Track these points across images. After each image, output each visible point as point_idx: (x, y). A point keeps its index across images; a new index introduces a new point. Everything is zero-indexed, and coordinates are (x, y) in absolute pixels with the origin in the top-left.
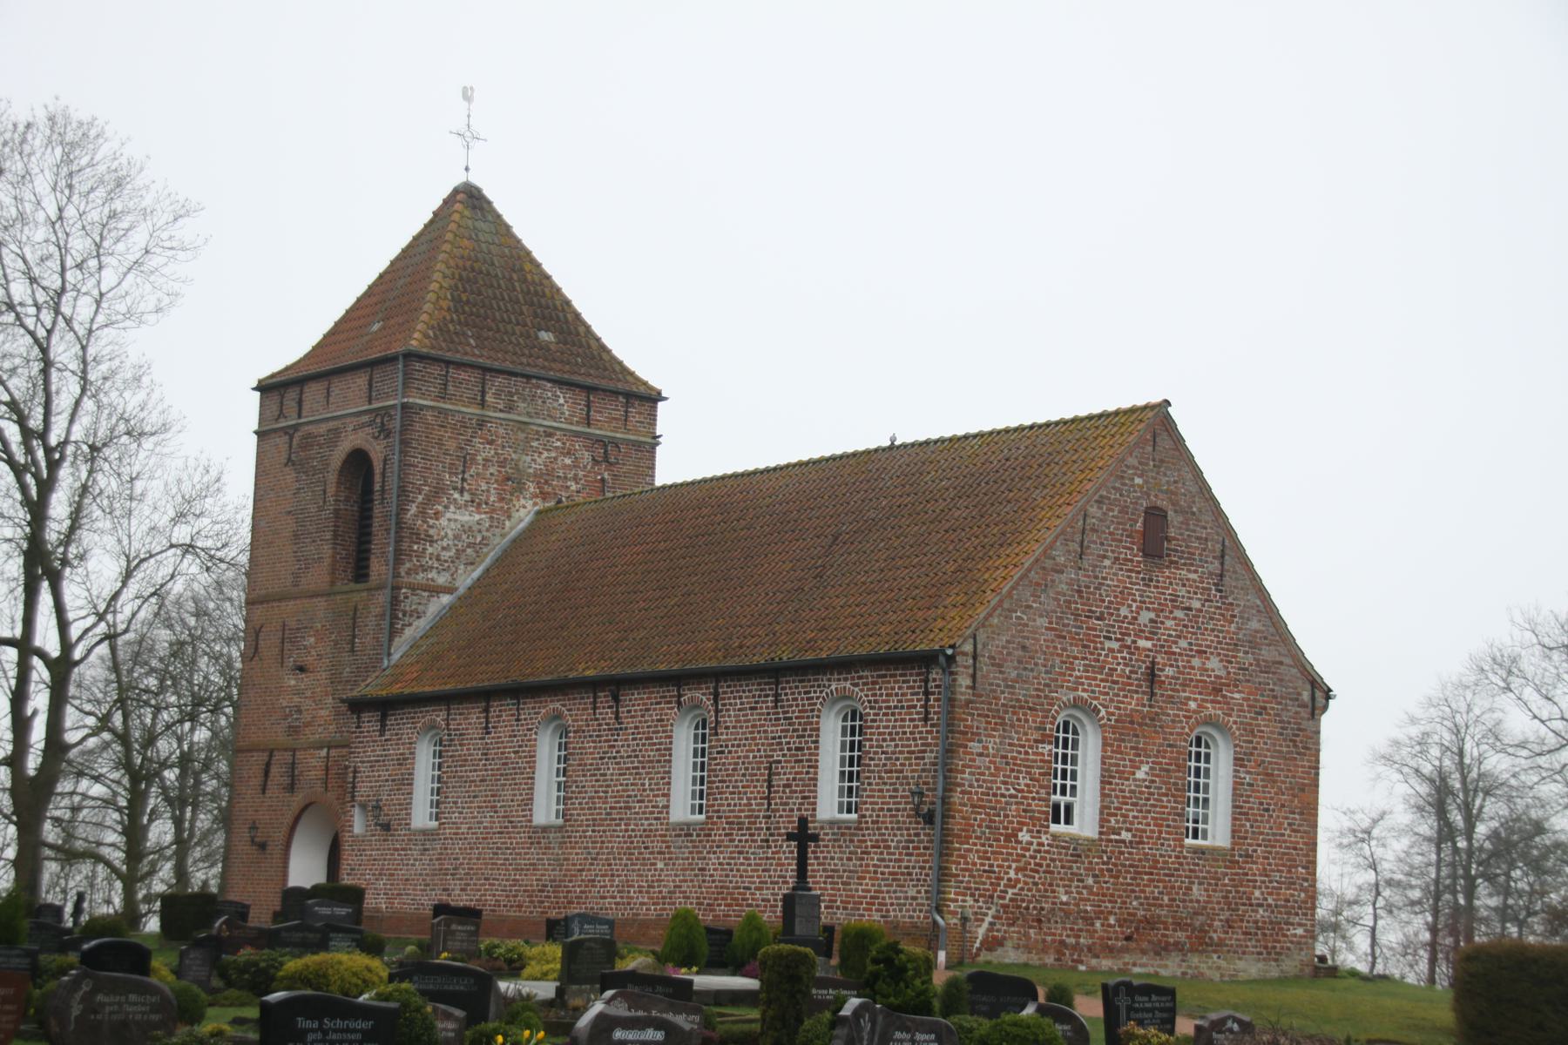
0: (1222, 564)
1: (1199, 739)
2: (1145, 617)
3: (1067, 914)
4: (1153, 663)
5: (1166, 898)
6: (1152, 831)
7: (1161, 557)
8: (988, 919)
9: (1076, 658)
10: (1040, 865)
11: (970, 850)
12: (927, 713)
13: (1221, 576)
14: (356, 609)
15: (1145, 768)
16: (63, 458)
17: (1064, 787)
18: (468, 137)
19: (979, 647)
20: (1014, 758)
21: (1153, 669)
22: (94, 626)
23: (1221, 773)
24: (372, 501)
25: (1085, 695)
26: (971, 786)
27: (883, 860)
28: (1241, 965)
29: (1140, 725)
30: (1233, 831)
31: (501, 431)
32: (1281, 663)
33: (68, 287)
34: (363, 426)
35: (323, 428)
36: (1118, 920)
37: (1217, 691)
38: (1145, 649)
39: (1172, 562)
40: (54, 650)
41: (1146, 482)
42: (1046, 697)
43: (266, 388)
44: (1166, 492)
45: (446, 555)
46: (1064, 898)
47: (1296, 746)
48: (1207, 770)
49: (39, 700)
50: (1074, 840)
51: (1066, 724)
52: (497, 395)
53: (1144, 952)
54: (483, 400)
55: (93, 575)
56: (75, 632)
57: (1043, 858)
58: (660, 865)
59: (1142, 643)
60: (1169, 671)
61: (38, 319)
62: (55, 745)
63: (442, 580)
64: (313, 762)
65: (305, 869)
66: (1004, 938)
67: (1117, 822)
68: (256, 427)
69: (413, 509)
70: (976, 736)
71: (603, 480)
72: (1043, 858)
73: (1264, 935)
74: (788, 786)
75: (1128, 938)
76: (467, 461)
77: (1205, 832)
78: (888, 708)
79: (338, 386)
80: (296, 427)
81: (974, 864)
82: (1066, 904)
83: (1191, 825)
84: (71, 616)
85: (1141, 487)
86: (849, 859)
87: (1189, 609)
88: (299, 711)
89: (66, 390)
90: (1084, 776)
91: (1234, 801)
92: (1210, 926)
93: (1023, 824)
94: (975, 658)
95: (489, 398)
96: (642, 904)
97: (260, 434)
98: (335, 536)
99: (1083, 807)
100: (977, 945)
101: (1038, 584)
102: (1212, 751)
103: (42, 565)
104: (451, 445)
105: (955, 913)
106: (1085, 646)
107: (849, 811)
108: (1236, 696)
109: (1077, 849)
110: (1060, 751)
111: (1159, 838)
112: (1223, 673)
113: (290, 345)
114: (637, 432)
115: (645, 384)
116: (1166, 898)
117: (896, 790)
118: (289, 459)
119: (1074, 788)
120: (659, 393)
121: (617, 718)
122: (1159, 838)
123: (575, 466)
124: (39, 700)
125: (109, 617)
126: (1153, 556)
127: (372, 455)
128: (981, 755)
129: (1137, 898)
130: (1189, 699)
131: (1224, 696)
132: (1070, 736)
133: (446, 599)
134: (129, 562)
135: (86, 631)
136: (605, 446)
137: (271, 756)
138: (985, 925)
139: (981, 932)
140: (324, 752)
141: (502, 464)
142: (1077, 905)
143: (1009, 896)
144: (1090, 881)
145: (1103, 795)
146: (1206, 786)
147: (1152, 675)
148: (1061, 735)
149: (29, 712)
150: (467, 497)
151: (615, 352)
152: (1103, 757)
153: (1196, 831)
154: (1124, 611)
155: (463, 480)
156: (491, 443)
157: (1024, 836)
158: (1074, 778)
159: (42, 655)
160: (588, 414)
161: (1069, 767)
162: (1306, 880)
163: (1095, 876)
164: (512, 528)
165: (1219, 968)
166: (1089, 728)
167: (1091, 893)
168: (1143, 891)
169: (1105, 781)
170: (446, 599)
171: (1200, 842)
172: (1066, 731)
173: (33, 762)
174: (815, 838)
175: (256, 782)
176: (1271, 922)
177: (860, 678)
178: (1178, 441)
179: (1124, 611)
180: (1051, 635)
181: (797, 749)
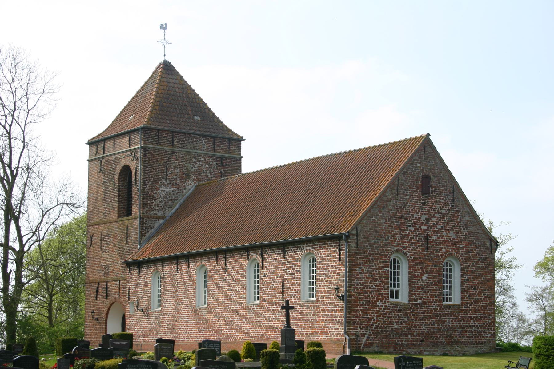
0: (453, 196)
1: (447, 263)
2: (424, 217)
3: (397, 333)
4: (428, 235)
5: (436, 325)
6: (430, 299)
7: (429, 194)
8: (367, 336)
9: (397, 234)
10: (386, 314)
11: (358, 310)
12: (340, 258)
13: (453, 200)
14: (127, 227)
15: (426, 275)
16: (17, 173)
17: (394, 284)
18: (165, 43)
19: (359, 231)
20: (374, 274)
21: (427, 237)
22: (32, 237)
23: (456, 276)
24: (132, 185)
25: (401, 248)
26: (358, 285)
27: (326, 315)
28: (466, 349)
29: (424, 259)
30: (462, 298)
31: (180, 155)
32: (478, 233)
33: (17, 108)
34: (128, 156)
35: (113, 158)
36: (417, 334)
37: (453, 244)
38: (424, 230)
39: (433, 196)
40: (17, 247)
41: (422, 165)
42: (386, 250)
43: (92, 143)
44: (430, 169)
45: (161, 204)
46: (396, 327)
47: (485, 264)
48: (451, 275)
49: (12, 266)
50: (399, 304)
51: (395, 260)
52: (178, 142)
53: (428, 346)
54: (173, 144)
55: (29, 219)
56: (24, 240)
57: (387, 312)
58: (244, 321)
59: (423, 227)
60: (434, 238)
61: (6, 121)
62: (19, 284)
63: (160, 214)
64: (114, 287)
65: (114, 328)
66: (373, 343)
67: (416, 296)
68: (88, 158)
69: (148, 187)
70: (359, 266)
71: (221, 172)
72: (387, 312)
73: (475, 337)
74: (290, 288)
75: (421, 341)
76: (167, 167)
77: (451, 299)
78: (326, 256)
79: (119, 141)
80: (103, 158)
81: (360, 315)
82: (397, 329)
83: (445, 296)
84: (23, 234)
85: (420, 167)
86: (313, 315)
87: (441, 213)
88: (108, 267)
89: (17, 146)
90: (402, 279)
91: (461, 286)
92: (454, 335)
93: (379, 299)
94: (357, 236)
95: (175, 143)
96: (238, 336)
97: (90, 161)
98: (119, 199)
99: (402, 291)
100: (362, 346)
101: (381, 207)
102: (452, 268)
103: (12, 215)
104: (161, 162)
105: (353, 334)
106: (400, 230)
107: (313, 297)
108: (461, 246)
109: (400, 307)
110: (393, 270)
111: (432, 302)
112: (455, 237)
113: (99, 127)
114: (234, 153)
115: (236, 134)
116: (436, 325)
117: (329, 288)
118: (101, 170)
119: (398, 284)
120: (242, 138)
121: (226, 265)
122: (432, 302)
123: (210, 167)
124: (12, 266)
125: (37, 233)
126: (426, 194)
127: (132, 167)
128: (361, 273)
129: (424, 325)
130: (442, 248)
131: (456, 246)
132: (396, 264)
133: (161, 221)
134: (43, 212)
135: (29, 239)
136: (222, 159)
137: (99, 284)
138: (365, 338)
139: (364, 340)
140: (118, 283)
141: (181, 168)
142: (401, 329)
143: (374, 327)
144: (406, 319)
145: (410, 286)
146: (451, 281)
147: (427, 239)
148: (393, 264)
149: (8, 271)
150: (168, 181)
151: (224, 123)
152: (409, 272)
153: (447, 298)
154: (415, 215)
155: (167, 175)
156: (177, 160)
157: (379, 304)
158: (451, 277)
159: (14, 250)
160: (214, 147)
161: (396, 276)
162: (491, 315)
163: (407, 318)
164: (186, 193)
165: (458, 351)
166: (404, 261)
167: (407, 324)
168: (427, 323)
169: (410, 281)
170: (161, 221)
171: (449, 303)
172: (394, 262)
173: (11, 289)
174: (292, 308)
175: (93, 295)
176: (478, 332)
177: (315, 245)
178: (434, 149)
179: (415, 215)
180: (387, 226)
181: (292, 274)
